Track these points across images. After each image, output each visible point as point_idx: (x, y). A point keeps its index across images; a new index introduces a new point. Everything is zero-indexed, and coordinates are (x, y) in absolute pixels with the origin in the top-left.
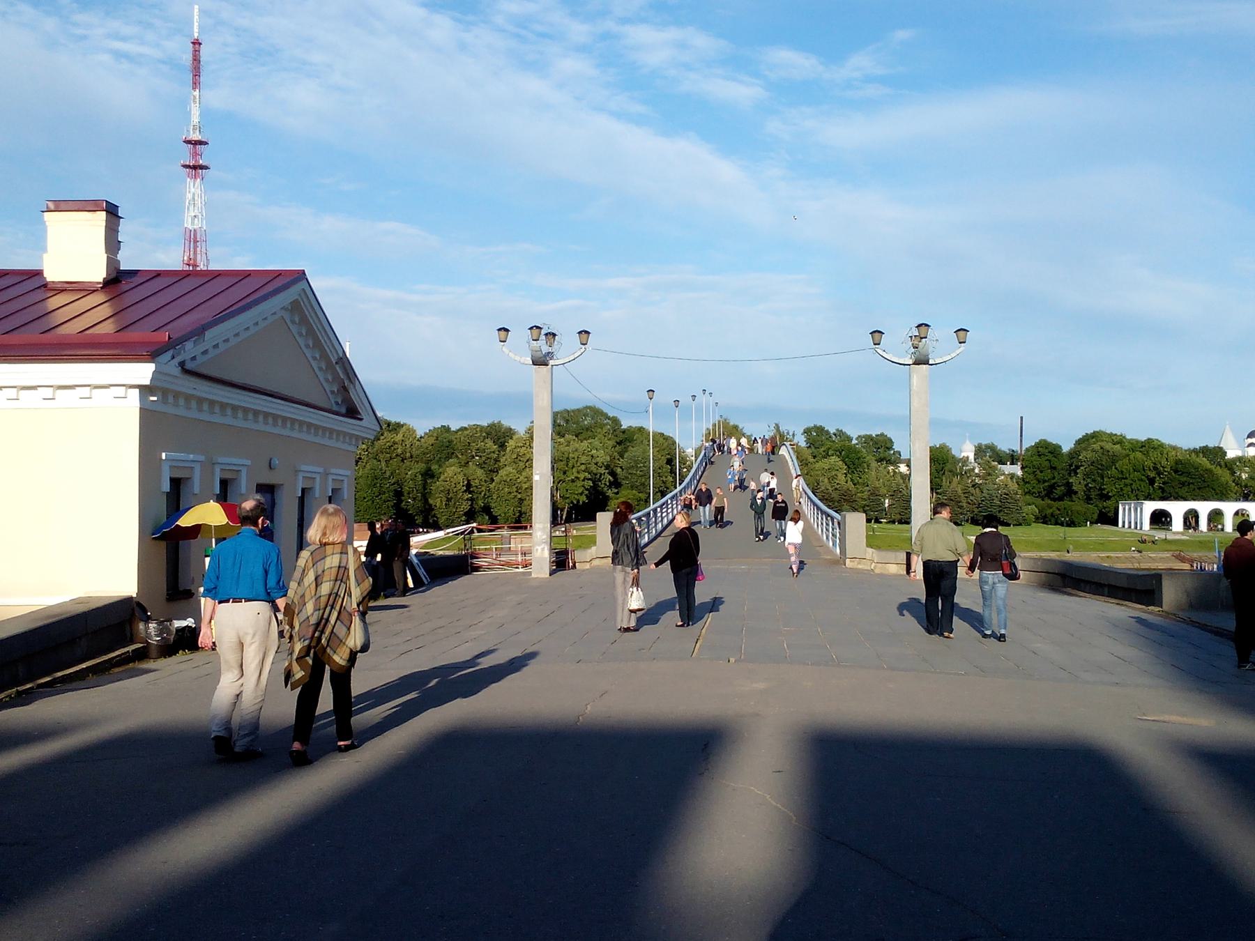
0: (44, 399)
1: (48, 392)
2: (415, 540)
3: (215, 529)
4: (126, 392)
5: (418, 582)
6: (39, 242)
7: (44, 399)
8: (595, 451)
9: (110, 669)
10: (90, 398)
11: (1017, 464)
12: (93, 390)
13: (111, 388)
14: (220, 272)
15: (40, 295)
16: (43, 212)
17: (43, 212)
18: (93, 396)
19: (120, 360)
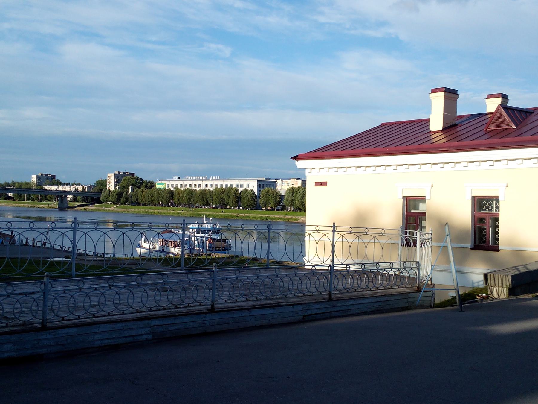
0: (477, 166)
1: (491, 163)
2: (108, 174)
3: (497, 247)
4: (522, 162)
5: (172, 205)
6: (485, 106)
7: (477, 166)
8: (249, 218)
9: (452, 298)
10: (507, 165)
11: (136, 176)
12: (387, 167)
13: (502, 161)
14: (405, 122)
15: (428, 135)
16: (485, 99)
17: (485, 99)
18: (397, 169)
19: (536, 147)
